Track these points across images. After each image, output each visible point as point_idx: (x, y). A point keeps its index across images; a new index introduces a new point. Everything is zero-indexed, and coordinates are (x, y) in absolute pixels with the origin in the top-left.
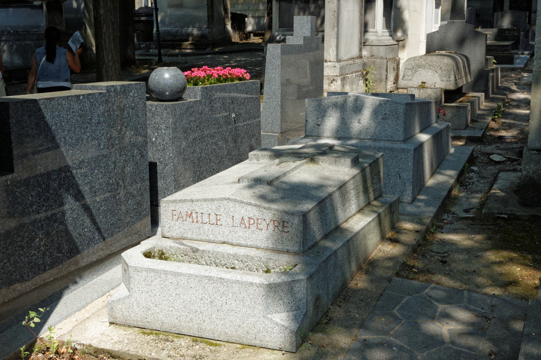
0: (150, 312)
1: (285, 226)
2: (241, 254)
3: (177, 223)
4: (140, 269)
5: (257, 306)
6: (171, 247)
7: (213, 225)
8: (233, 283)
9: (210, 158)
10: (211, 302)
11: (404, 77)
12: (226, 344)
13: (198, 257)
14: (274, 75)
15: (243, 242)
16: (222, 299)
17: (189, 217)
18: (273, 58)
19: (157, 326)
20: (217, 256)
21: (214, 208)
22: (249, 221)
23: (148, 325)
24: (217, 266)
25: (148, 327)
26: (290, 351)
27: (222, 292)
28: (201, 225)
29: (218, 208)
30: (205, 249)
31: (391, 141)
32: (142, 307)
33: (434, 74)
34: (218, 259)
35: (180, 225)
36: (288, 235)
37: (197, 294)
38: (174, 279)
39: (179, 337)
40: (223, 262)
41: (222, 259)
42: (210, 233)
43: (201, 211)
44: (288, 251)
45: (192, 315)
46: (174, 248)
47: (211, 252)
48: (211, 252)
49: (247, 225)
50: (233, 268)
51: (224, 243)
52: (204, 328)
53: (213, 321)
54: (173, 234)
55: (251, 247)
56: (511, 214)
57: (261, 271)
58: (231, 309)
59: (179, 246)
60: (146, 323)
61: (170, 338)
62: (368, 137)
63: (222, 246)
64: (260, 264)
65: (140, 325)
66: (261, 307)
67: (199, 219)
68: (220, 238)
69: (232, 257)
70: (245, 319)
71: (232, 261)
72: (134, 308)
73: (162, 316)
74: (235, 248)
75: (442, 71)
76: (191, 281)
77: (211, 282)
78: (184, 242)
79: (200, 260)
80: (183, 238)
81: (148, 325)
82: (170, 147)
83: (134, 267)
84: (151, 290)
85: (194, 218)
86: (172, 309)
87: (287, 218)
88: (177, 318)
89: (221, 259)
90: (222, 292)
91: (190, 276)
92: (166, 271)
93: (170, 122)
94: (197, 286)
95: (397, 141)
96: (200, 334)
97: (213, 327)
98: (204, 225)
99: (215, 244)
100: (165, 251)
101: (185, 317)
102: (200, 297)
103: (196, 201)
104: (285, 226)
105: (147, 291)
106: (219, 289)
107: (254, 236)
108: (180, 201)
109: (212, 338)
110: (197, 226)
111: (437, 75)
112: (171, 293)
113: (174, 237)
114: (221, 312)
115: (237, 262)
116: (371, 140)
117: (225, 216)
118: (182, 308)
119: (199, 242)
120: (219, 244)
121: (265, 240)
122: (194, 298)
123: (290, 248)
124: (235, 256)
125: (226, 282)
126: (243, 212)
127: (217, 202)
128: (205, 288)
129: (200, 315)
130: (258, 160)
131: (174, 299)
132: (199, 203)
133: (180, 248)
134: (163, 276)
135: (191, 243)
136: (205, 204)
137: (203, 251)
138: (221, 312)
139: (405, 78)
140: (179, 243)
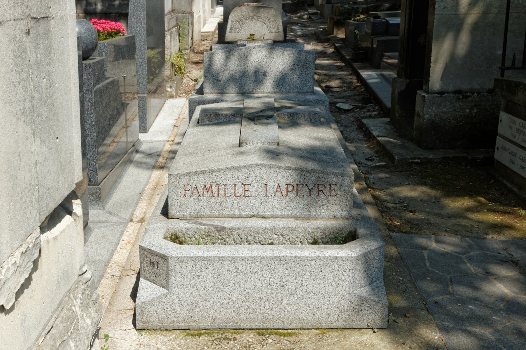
0: (197, 309)
2: (281, 226)
3: (191, 200)
4: (185, 259)
5: (342, 283)
6: (188, 229)
7: (239, 198)
8: (312, 260)
10: (282, 286)
11: (231, 29)
12: (301, 332)
13: (224, 237)
14: (138, 29)
15: (277, 213)
16: (296, 281)
17: (208, 192)
18: (137, 10)
19: (207, 324)
20: (250, 233)
21: (241, 177)
22: (287, 188)
23: (193, 325)
24: (249, 244)
25: (194, 327)
26: (380, 327)
27: (296, 272)
28: (223, 199)
30: (232, 225)
31: (300, 93)
32: (185, 305)
33: (262, 25)
34: (251, 236)
35: (195, 201)
36: (335, 199)
37: (263, 279)
38: (232, 265)
39: (239, 333)
40: (257, 238)
41: (256, 235)
42: (235, 207)
44: (335, 217)
45: (255, 304)
46: (191, 230)
47: (242, 228)
48: (242, 228)
49: (284, 193)
50: (272, 244)
51: (254, 216)
52: (271, 317)
53: (283, 308)
54: (185, 214)
55: (288, 217)
56: (423, 158)
57: (307, 243)
58: (308, 290)
59: (198, 226)
60: (192, 323)
61: (229, 335)
62: (275, 91)
63: (251, 221)
64: (304, 235)
65: (183, 325)
67: (222, 192)
68: (249, 212)
69: (269, 231)
70: (326, 300)
71: (269, 236)
72: (174, 307)
73: (213, 311)
74: (269, 221)
75: (270, 22)
76: (256, 265)
77: (283, 263)
78: (200, 220)
79: (228, 239)
80: (199, 216)
81: (194, 325)
82: (92, 113)
83: (176, 258)
84: (200, 283)
86: (227, 301)
87: (334, 179)
88: (234, 311)
89: (255, 235)
90: (296, 272)
91: (255, 258)
92: (222, 257)
93: (92, 84)
95: (307, 92)
96: (265, 325)
97: (282, 315)
98: (228, 199)
99: (241, 219)
100: (179, 235)
101: (246, 308)
102: (268, 282)
103: (217, 171)
104: (332, 189)
105: (194, 284)
106: (294, 269)
107: (292, 205)
108: (196, 173)
109: (281, 328)
110: (218, 201)
111: (265, 26)
112: (227, 283)
113: (186, 217)
114: (295, 296)
115: (275, 236)
116: (278, 93)
117: (255, 185)
118: (241, 299)
119: (220, 219)
120: (247, 219)
123: (338, 214)
124: (273, 230)
125: (303, 261)
126: (279, 178)
127: (246, 170)
128: (274, 270)
129: (267, 303)
130: (211, 121)
131: (231, 289)
132: (222, 174)
133: (200, 229)
134: (217, 264)
135: (210, 221)
136: (229, 174)
137: (232, 229)
138: (295, 296)
139: (233, 31)
140: (196, 223)
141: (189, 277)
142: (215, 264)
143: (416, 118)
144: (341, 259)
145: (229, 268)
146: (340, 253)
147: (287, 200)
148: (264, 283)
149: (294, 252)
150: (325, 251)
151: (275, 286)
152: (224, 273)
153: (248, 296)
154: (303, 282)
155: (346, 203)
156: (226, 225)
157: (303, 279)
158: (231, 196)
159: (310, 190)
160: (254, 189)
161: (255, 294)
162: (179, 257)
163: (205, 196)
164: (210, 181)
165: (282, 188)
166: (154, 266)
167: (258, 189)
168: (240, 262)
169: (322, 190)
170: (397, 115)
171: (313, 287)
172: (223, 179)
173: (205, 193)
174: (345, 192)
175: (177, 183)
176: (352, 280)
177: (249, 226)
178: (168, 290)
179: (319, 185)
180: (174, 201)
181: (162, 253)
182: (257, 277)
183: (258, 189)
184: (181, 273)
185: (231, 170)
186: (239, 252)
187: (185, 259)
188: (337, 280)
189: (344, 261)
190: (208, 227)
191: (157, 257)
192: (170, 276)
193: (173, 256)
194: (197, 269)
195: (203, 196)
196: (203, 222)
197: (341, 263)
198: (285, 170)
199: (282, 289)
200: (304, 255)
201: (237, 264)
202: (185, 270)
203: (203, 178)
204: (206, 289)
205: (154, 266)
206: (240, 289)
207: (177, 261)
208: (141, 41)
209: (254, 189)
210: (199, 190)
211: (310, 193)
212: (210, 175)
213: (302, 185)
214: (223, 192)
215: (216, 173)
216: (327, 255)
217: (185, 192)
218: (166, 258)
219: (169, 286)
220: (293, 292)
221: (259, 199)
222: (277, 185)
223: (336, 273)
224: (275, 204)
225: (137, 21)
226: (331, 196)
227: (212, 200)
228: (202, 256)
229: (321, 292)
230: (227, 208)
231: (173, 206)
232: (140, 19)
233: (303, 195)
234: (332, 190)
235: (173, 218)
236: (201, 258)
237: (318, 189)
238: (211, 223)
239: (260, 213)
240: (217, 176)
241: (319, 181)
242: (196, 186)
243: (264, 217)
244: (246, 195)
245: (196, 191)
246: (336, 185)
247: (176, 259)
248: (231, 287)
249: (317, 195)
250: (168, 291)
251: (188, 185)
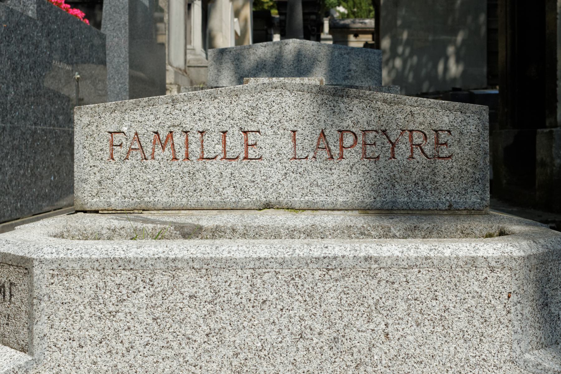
1: (441, 141)
2: (330, 225)
3: (125, 167)
4: (77, 266)
5: (490, 331)
6: (114, 230)
7: (234, 162)
8: (411, 267)
9: (48, 140)
14: (116, 39)
15: (321, 199)
16: (372, 326)
17: (163, 148)
18: (115, 11)
21: (237, 114)
22: (342, 140)
27: (371, 302)
28: (199, 166)
29: (250, 115)
35: (135, 171)
36: (450, 165)
37: (284, 321)
38: (202, 282)
42: (225, 183)
43: (201, 126)
44: (450, 206)
46: (122, 232)
49: (336, 151)
51: (268, 206)
54: (113, 200)
58: (403, 351)
66: (502, 333)
67: (194, 147)
74: (303, 216)
77: (335, 274)
78: (146, 215)
80: (144, 206)
83: (52, 262)
84: (117, 332)
85: (177, 147)
87: (446, 119)
90: (371, 302)
92: (174, 260)
94: (285, 295)
98: (208, 164)
99: (240, 212)
102: (296, 329)
105: (100, 337)
106: (364, 293)
110: (186, 170)
112: (189, 332)
119: (191, 212)
120: (253, 211)
121: (385, 184)
122: (274, 335)
123: (457, 199)
128: (311, 297)
131: (200, 351)
141: (87, 317)
142: (157, 278)
143: (538, 170)
144: (485, 265)
145: (195, 290)
146: (482, 248)
147: (341, 167)
148: (286, 331)
149: (363, 247)
150: (442, 245)
151: (315, 340)
152: (181, 305)
153: (245, 369)
154: (390, 329)
155: (474, 173)
156: (204, 223)
157: (390, 322)
158: (215, 158)
159: (393, 144)
160: (268, 141)
161: (265, 364)
162: (62, 259)
163: (157, 157)
164: (169, 124)
165: (331, 140)
166: (4, 296)
167: (277, 141)
168: (223, 274)
169: (419, 145)
170: (505, 181)
171: (416, 344)
172: (197, 118)
173: (158, 151)
174: (471, 149)
175: (94, 128)
176: (516, 323)
177: (255, 225)
178: (32, 354)
179: (411, 131)
180: (87, 170)
181: (21, 254)
182: (267, 315)
183: (277, 141)
184: (66, 306)
185: (216, 98)
186: (221, 249)
187: (77, 266)
188: (477, 324)
189: (492, 271)
190: (162, 226)
191: (11, 269)
192: (37, 314)
193: (46, 256)
194: (108, 293)
195: (153, 158)
196: (152, 218)
197: (485, 275)
198: (336, 98)
199: (335, 350)
200: (389, 254)
201: (214, 278)
202: (77, 298)
203: (152, 116)
204: (132, 351)
205: (4, 296)
206: (223, 350)
207: (56, 273)
208: (120, 57)
209: (268, 141)
210: (143, 144)
211: (393, 151)
212: (169, 110)
213: (374, 133)
214: (199, 150)
215: (182, 104)
216: (447, 253)
217: (113, 150)
218: (28, 265)
219: (35, 342)
220: (363, 357)
221: (279, 164)
222: (319, 132)
223: (473, 302)
224: (315, 178)
225: (115, 27)
226: (439, 157)
227: (174, 168)
228: (122, 256)
229: (438, 358)
230: (208, 186)
231: (85, 181)
232: (119, 25)
233: (377, 155)
234: (442, 144)
235: (85, 212)
236: (121, 263)
237: (412, 141)
238: (171, 219)
239: (281, 199)
240: (185, 111)
241: (411, 124)
242: (136, 134)
243: (290, 208)
244: (250, 156)
245: (137, 146)
246: (449, 131)
247: (54, 267)
248: (200, 346)
249: (409, 154)
250: (30, 358)
251: (119, 132)
